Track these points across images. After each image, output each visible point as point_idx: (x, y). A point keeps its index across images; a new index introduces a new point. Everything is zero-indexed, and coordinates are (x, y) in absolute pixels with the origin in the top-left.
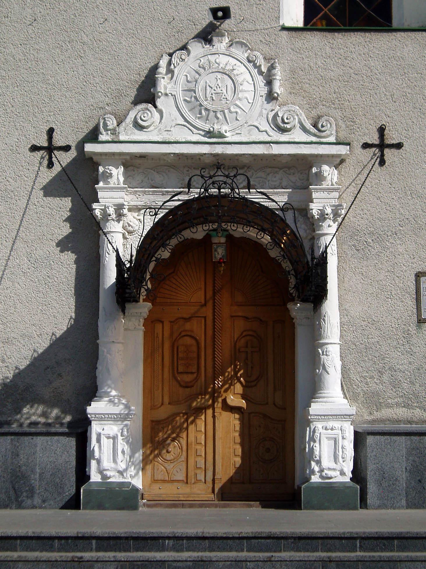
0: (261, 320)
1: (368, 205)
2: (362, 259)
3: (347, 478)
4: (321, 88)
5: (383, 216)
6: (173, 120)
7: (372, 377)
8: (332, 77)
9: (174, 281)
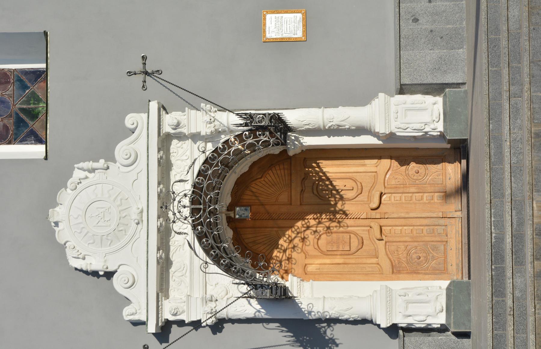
0: (304, 179)
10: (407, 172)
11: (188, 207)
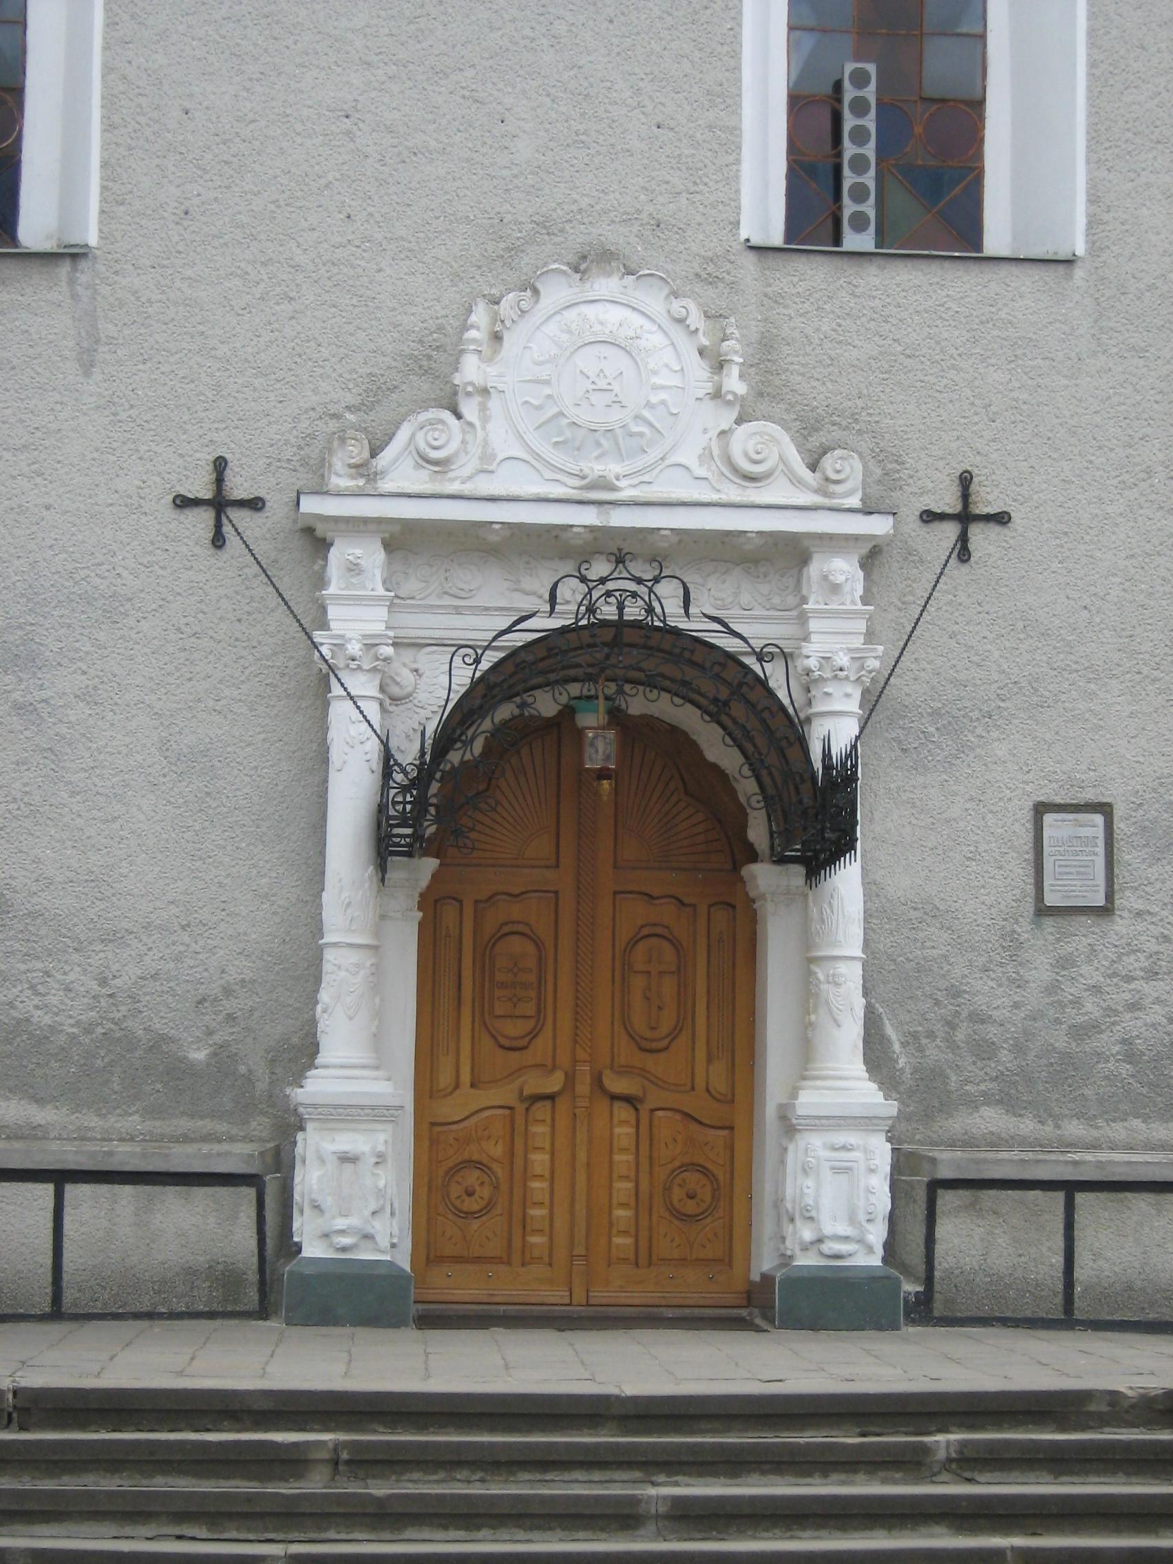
3: (876, 1260)
4: (829, 384)
8: (856, 362)
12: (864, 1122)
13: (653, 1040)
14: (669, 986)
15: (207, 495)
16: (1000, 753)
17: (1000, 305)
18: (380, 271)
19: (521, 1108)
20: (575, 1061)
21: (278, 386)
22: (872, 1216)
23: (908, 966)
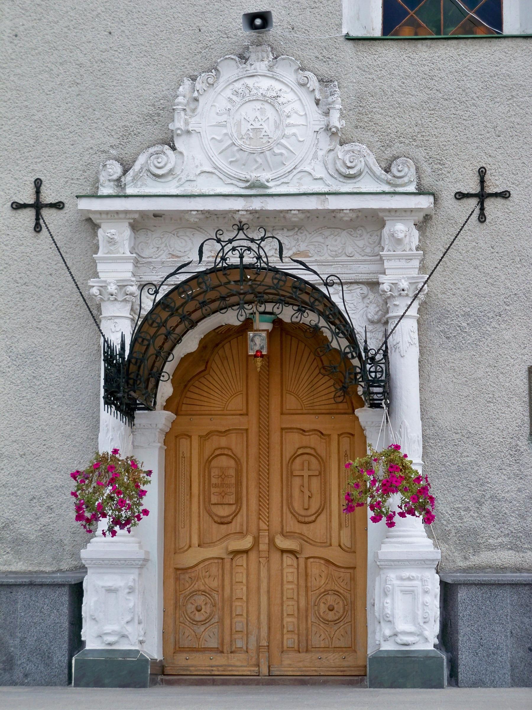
1: (462, 277)
2: (454, 350)
4: (397, 119)
5: (482, 292)
6: (197, 167)
7: (467, 509)
8: (414, 105)
9: (206, 383)
10: (330, 592)
11: (241, 261)
12: (421, 563)
13: (305, 516)
14: (315, 483)
15: (32, 201)
16: (507, 338)
17: (501, 66)
18: (129, 64)
19: (228, 558)
20: (259, 530)
21: (71, 135)
22: (427, 619)
23: (453, 468)
